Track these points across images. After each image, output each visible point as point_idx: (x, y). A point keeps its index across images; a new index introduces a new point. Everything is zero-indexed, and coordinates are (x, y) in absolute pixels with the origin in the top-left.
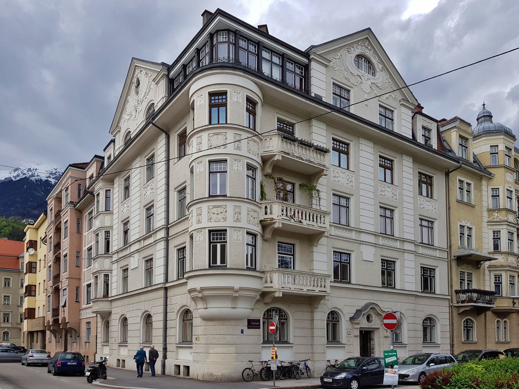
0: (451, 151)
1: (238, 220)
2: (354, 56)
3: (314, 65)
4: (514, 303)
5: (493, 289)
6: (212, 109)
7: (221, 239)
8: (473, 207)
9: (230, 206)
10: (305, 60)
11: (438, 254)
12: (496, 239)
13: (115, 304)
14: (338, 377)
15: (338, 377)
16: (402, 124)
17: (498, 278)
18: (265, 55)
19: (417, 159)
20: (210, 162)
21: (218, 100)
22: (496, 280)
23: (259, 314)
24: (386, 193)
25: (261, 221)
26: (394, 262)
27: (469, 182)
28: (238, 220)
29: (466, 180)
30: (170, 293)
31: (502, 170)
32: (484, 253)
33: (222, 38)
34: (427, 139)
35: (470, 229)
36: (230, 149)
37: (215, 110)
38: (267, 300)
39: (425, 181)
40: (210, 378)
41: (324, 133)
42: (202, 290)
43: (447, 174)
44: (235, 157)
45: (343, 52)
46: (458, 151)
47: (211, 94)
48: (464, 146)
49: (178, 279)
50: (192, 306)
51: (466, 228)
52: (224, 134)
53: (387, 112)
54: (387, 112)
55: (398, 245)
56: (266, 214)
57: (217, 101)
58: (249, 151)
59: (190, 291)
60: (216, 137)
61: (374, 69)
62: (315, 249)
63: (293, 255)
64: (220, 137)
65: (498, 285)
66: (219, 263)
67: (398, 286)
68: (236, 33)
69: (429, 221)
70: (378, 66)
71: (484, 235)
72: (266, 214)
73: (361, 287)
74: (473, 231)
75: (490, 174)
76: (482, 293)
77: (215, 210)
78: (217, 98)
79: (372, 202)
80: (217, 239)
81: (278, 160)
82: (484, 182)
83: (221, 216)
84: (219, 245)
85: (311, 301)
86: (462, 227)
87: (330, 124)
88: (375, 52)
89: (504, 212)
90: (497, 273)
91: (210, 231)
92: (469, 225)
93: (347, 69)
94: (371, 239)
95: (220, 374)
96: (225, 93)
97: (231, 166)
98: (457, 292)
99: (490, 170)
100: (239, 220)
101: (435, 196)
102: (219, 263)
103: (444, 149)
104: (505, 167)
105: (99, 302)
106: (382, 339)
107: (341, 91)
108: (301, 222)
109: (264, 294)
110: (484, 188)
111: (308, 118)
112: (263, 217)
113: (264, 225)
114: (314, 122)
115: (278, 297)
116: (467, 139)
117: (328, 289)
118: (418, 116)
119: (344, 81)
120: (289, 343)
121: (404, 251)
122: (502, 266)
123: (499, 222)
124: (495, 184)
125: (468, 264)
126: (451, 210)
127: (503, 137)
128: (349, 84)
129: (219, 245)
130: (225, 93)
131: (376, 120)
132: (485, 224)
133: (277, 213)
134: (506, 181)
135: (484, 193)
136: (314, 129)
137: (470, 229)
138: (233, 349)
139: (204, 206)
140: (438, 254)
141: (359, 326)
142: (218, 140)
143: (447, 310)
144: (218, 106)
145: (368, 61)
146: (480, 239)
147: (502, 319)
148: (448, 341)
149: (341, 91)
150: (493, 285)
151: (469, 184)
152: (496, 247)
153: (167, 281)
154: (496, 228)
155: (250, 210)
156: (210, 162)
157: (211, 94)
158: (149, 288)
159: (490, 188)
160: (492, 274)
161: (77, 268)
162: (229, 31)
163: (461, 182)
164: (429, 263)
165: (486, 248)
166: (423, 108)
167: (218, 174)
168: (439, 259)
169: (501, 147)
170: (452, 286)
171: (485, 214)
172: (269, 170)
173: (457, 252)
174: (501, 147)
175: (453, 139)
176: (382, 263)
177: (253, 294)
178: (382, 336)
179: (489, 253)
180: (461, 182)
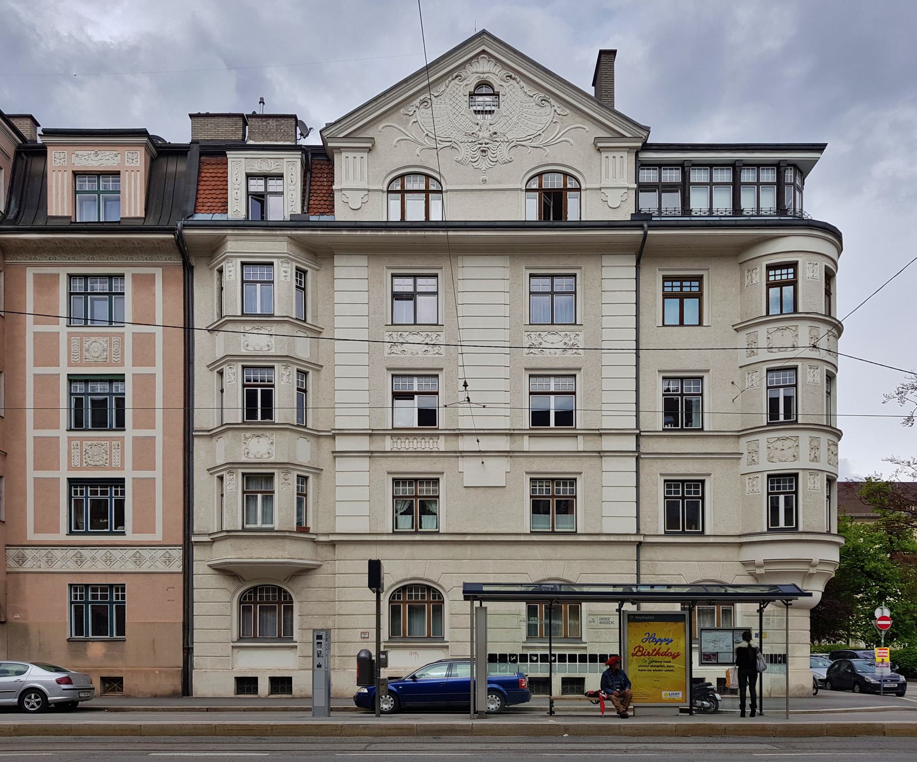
6: (770, 290)
7: (785, 488)
9: (804, 437)
14: (748, 687)
15: (748, 687)
20: (768, 370)
22: (669, 492)
28: (815, 459)
40: (801, 692)
42: (767, 562)
52: (794, 328)
57: (778, 278)
59: (745, 564)
60: (780, 333)
64: (786, 332)
66: (782, 524)
73: (469, 538)
77: (779, 444)
78: (778, 272)
80: (778, 488)
84: (782, 498)
91: (769, 476)
94: (363, 444)
97: (805, 378)
102: (782, 524)
105: (287, 542)
129: (782, 498)
142: (782, 338)
155: (830, 443)
156: (768, 370)
167: (258, 285)
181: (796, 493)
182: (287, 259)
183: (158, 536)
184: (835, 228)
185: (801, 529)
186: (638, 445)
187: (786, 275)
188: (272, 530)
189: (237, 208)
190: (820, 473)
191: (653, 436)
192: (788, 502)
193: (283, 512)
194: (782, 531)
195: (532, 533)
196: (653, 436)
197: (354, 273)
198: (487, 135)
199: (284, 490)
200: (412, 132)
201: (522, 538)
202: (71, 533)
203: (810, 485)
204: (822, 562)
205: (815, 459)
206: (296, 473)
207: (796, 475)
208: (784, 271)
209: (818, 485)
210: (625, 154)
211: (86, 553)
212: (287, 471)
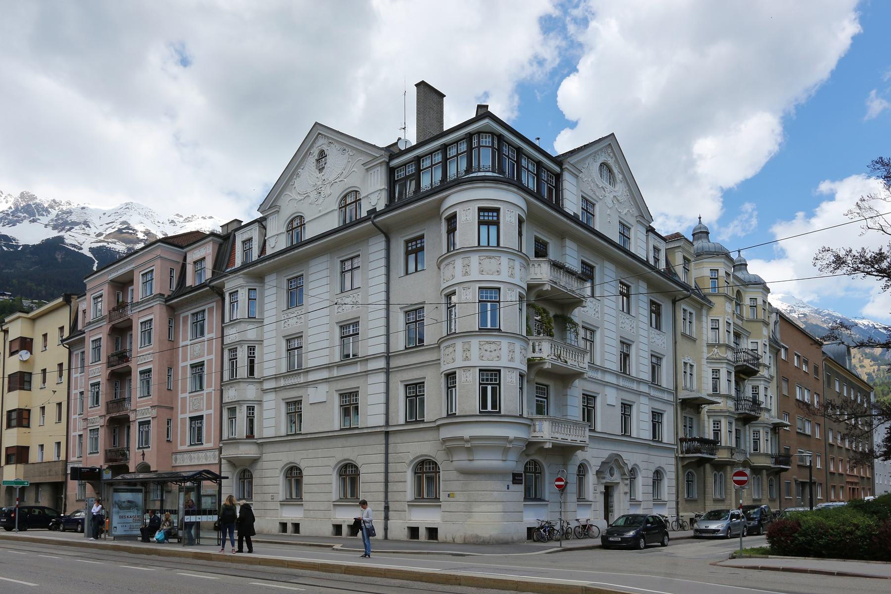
0: (675, 274)
1: (512, 359)
2: (599, 164)
3: (567, 176)
4: (732, 454)
5: (712, 438)
7: (491, 380)
8: (694, 340)
9: (505, 343)
10: (557, 169)
11: (666, 396)
12: (716, 379)
13: (267, 449)
16: (639, 246)
17: (717, 423)
18: (524, 162)
19: (653, 286)
21: (489, 217)
23: (520, 469)
24: (655, 339)
25: (529, 360)
26: (594, 397)
27: (692, 311)
29: (689, 310)
30: (392, 439)
31: (722, 299)
32: (704, 395)
33: (486, 141)
34: (657, 260)
35: (692, 366)
36: (504, 277)
37: (484, 229)
38: (532, 450)
39: (655, 309)
41: (575, 255)
42: (472, 438)
43: (674, 302)
44: (509, 286)
45: (590, 160)
46: (682, 277)
47: (481, 210)
48: (686, 270)
49: (407, 423)
50: (440, 458)
51: (688, 366)
53: (625, 228)
54: (625, 228)
55: (635, 386)
56: (534, 351)
57: (486, 218)
58: (481, 272)
60: (488, 260)
61: (614, 177)
62: (569, 392)
63: (547, 398)
64: (492, 260)
65: (717, 433)
66: (489, 408)
67: (634, 434)
68: (500, 137)
69: (657, 357)
70: (619, 177)
71: (704, 374)
72: (534, 351)
73: (309, 436)
74: (695, 368)
75: (710, 302)
76: (703, 441)
77: (487, 347)
78: (486, 214)
79: (614, 335)
81: (547, 290)
82: (704, 312)
83: (494, 354)
84: (489, 388)
85: (564, 452)
86: (685, 364)
87: (582, 243)
88: (617, 161)
89: (723, 349)
90: (717, 418)
91: (480, 370)
92: (690, 362)
93: (593, 181)
95: (487, 536)
96: (497, 210)
98: (682, 440)
99: (710, 298)
100: (509, 357)
101: (664, 328)
102: (489, 408)
103: (669, 273)
104: (726, 296)
106: (622, 495)
107: (588, 204)
108: (566, 362)
109: (530, 444)
110: (704, 318)
111: (562, 235)
112: (531, 355)
113: (531, 363)
114: (569, 243)
115: (548, 449)
116: (689, 261)
117: (587, 439)
118: (650, 233)
119: (591, 194)
120: (544, 501)
121: (607, 384)
122: (721, 411)
123: (719, 360)
124: (714, 314)
125: (691, 408)
126: (678, 344)
127: (723, 260)
128: (595, 197)
129: (489, 388)
130: (497, 210)
131: (616, 239)
132: (704, 361)
133: (545, 350)
134: (726, 313)
135: (704, 325)
136: (568, 251)
137: (692, 366)
138: (500, 507)
139: (475, 342)
140: (666, 396)
141: (604, 481)
142: (490, 264)
143: (673, 461)
144: (488, 223)
145: (610, 171)
146: (700, 378)
147: (719, 472)
148: (674, 497)
149: (588, 204)
150: (712, 433)
151: (691, 314)
152: (715, 388)
153: (387, 424)
154: (716, 366)
157: (481, 210)
158: (349, 431)
159: (709, 319)
160: (711, 421)
161: (168, 392)
162: (493, 134)
163: (685, 310)
164: (659, 406)
165: (705, 390)
166: (487, 106)
168: (666, 402)
169: (722, 273)
170: (677, 434)
171: (705, 349)
172: (532, 299)
173: (683, 395)
174: (722, 273)
175: (678, 260)
176: (583, 398)
177: (517, 444)
178: (622, 491)
179: (709, 395)
180: (685, 310)
181: (499, 384)
182: (242, 287)
183: (211, 445)
184: (198, 232)
185: (502, 413)
186: (388, 364)
187: (491, 217)
188: (235, 439)
189: (238, 262)
190: (472, 369)
191: (399, 355)
192: (494, 390)
193: (241, 429)
194: (489, 414)
195: (342, 430)
196: (399, 355)
197: (319, 275)
198: (320, 183)
199: (242, 415)
200: (294, 195)
201: (336, 434)
202: (191, 445)
203: (463, 379)
204: (516, 439)
205: (467, 358)
206: (245, 406)
207: (499, 371)
208: (490, 214)
209: (470, 379)
210: (379, 168)
211: (193, 455)
212: (241, 405)
